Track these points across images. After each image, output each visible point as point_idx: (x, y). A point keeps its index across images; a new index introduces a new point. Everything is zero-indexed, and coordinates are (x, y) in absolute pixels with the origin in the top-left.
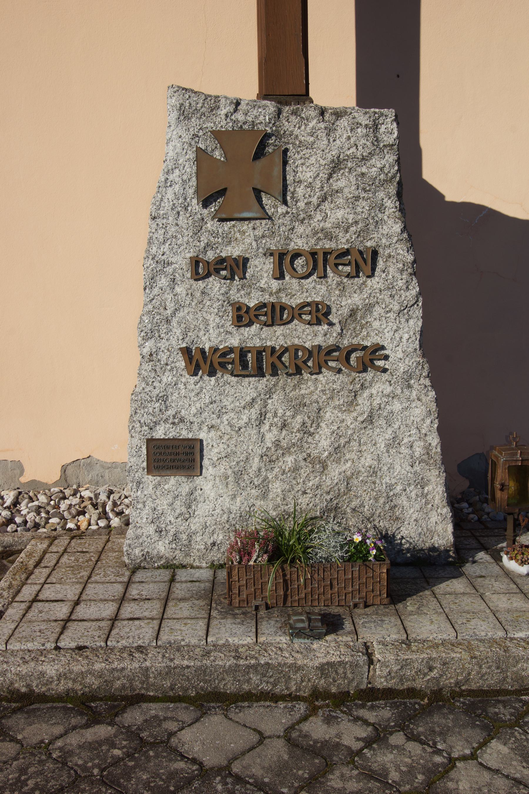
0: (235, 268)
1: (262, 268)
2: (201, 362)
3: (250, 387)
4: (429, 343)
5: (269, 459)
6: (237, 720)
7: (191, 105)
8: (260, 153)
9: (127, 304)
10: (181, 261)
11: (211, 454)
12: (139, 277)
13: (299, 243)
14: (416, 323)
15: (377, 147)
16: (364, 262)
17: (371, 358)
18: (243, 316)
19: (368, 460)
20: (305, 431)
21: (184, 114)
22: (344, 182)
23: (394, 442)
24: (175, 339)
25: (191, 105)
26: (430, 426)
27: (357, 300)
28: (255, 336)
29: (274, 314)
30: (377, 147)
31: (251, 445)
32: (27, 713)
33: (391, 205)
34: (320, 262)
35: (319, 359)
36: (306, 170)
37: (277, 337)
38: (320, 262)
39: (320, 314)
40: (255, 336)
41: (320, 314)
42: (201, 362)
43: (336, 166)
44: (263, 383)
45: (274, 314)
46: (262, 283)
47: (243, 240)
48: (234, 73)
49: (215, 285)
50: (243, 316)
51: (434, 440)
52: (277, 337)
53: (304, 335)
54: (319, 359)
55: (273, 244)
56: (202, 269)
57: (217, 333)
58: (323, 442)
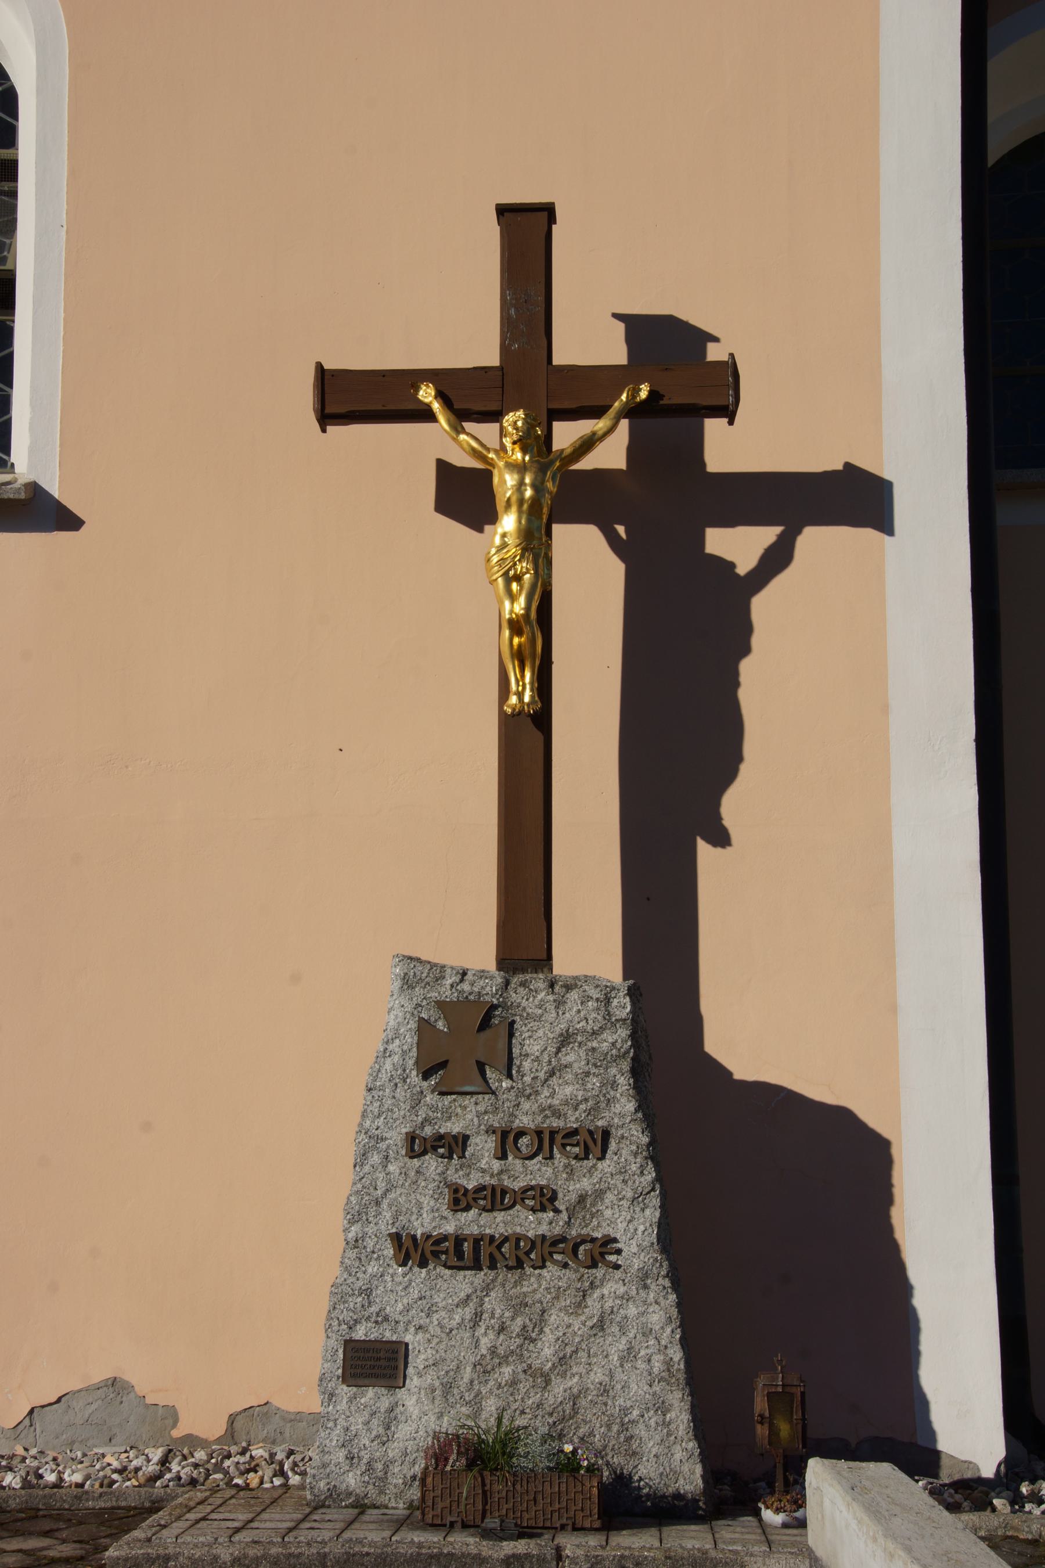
0: (454, 1146)
1: (483, 1146)
2: (412, 1250)
3: (465, 1282)
4: (669, 1237)
5: (482, 1369)
7: (417, 973)
8: (485, 1024)
9: (338, 1182)
10: (396, 1137)
11: (417, 1362)
12: (349, 1153)
13: (524, 1121)
14: (652, 1213)
15: (610, 1021)
18: (460, 1200)
19: (598, 1376)
20: (527, 1337)
21: (407, 983)
22: (569, 1056)
23: (629, 1354)
24: (384, 1223)
25: (417, 973)
26: (670, 1334)
27: (585, 1184)
28: (472, 1222)
29: (495, 1198)
30: (610, 1021)
31: (463, 1353)
33: (624, 1082)
34: (546, 1141)
36: (533, 1043)
38: (546, 1141)
39: (544, 1199)
40: (472, 1222)
41: (544, 1199)
42: (412, 1250)
43: (565, 1039)
44: (479, 1278)
45: (495, 1198)
46: (483, 1164)
47: (465, 1116)
48: (472, 944)
49: (432, 1164)
51: (676, 1354)
53: (529, 1223)
55: (496, 1121)
56: (418, 1146)
57: (430, 1218)
58: (546, 1351)
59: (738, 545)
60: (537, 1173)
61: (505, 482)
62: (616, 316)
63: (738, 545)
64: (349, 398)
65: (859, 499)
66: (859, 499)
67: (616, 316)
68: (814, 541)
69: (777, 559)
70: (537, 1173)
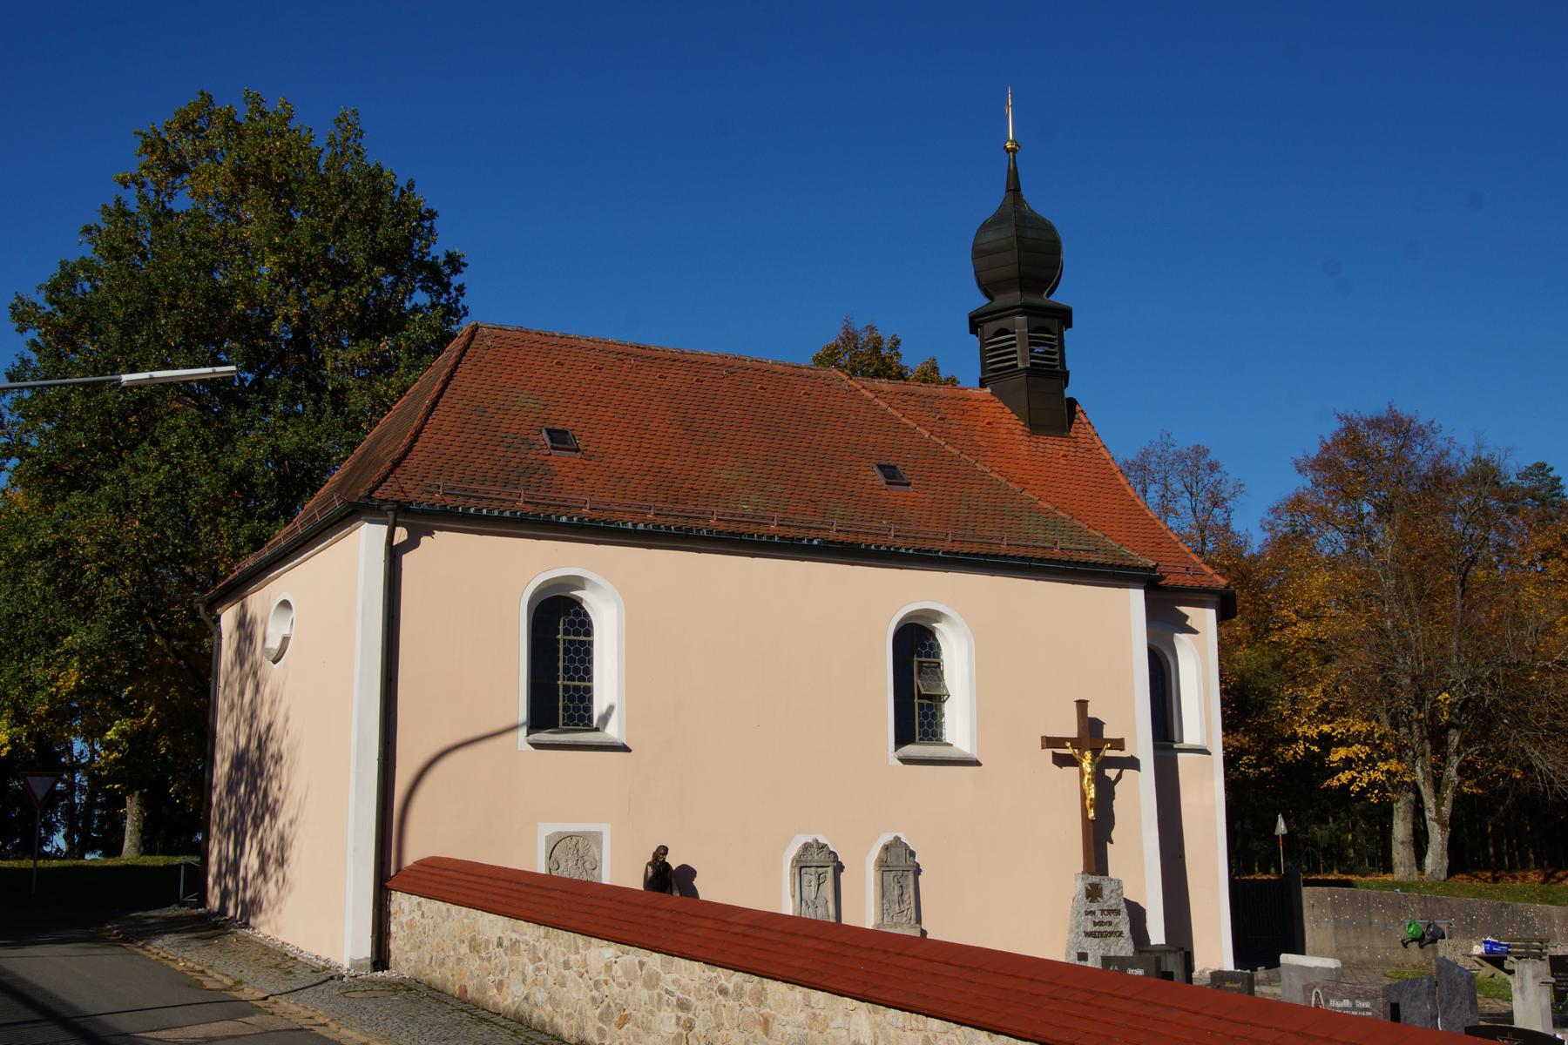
0: (1093, 913)
1: (1098, 913)
2: (1088, 934)
6: (388, 464)
16: (1118, 912)
17: (1120, 934)
18: (1095, 924)
28: (1097, 928)
29: (1101, 923)
32: (199, 985)
34: (1110, 912)
35: (1111, 933)
36: (1106, 892)
37: (1102, 929)
38: (1110, 912)
39: (1110, 923)
40: (1097, 928)
41: (1110, 923)
42: (1088, 934)
45: (1101, 923)
46: (1099, 917)
47: (1094, 907)
50: (1095, 924)
52: (1102, 929)
53: (1109, 929)
54: (1111, 933)
56: (1087, 913)
57: (1091, 928)
59: (1111, 773)
60: (1107, 918)
61: (65, 837)
62: (1195, 632)
63: (1111, 773)
64: (1049, 742)
65: (1133, 763)
66: (1133, 763)
67: (1195, 632)
68: (1126, 772)
69: (1119, 777)
70: (1107, 918)
